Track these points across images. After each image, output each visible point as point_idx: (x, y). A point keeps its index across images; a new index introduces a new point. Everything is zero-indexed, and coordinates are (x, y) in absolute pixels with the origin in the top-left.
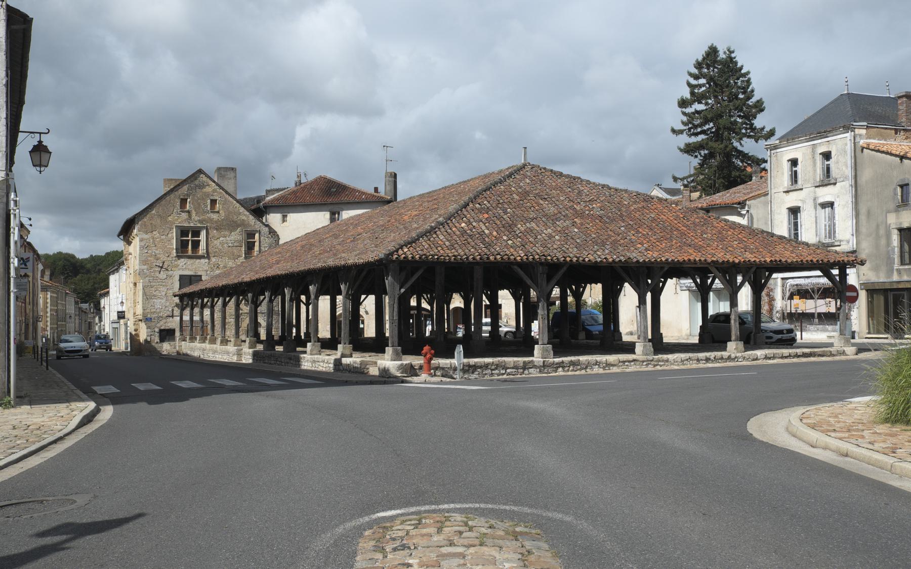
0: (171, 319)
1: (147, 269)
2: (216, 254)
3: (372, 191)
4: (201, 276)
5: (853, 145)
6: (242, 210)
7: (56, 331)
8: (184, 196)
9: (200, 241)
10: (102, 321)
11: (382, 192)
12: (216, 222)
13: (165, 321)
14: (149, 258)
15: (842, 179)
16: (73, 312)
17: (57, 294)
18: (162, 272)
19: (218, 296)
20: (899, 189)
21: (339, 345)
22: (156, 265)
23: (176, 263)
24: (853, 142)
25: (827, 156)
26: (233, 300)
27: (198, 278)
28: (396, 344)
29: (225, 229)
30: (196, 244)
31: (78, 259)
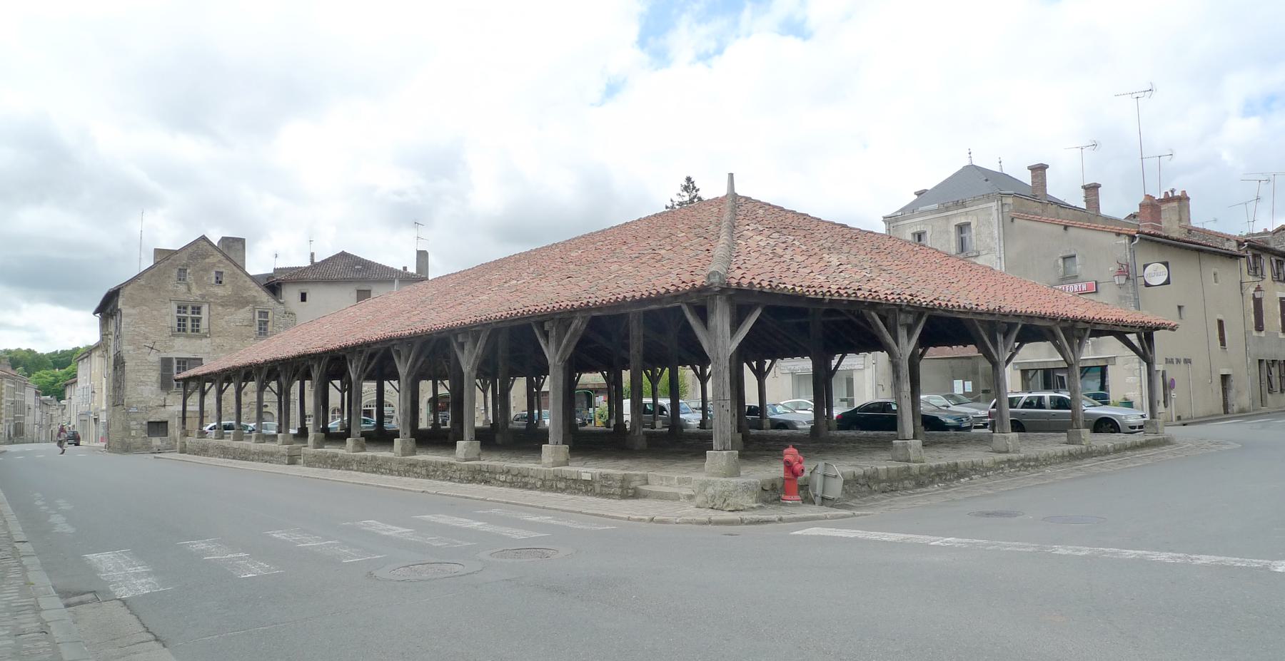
0: (163, 409)
1: (134, 350)
2: (221, 334)
3: (402, 269)
4: (201, 359)
5: (1000, 216)
6: (253, 285)
7: (13, 424)
8: (183, 266)
9: (201, 318)
10: (430, 401)
11: (412, 269)
12: (222, 297)
13: (155, 411)
14: (136, 338)
15: (986, 252)
16: (34, 404)
17: (14, 384)
18: (151, 354)
19: (229, 380)
20: (1060, 262)
21: (395, 439)
22: (145, 346)
23: (171, 344)
24: (1000, 211)
25: (962, 228)
26: (214, 387)
27: (198, 362)
28: (560, 441)
29: (232, 305)
30: (196, 321)
31: (42, 354)
